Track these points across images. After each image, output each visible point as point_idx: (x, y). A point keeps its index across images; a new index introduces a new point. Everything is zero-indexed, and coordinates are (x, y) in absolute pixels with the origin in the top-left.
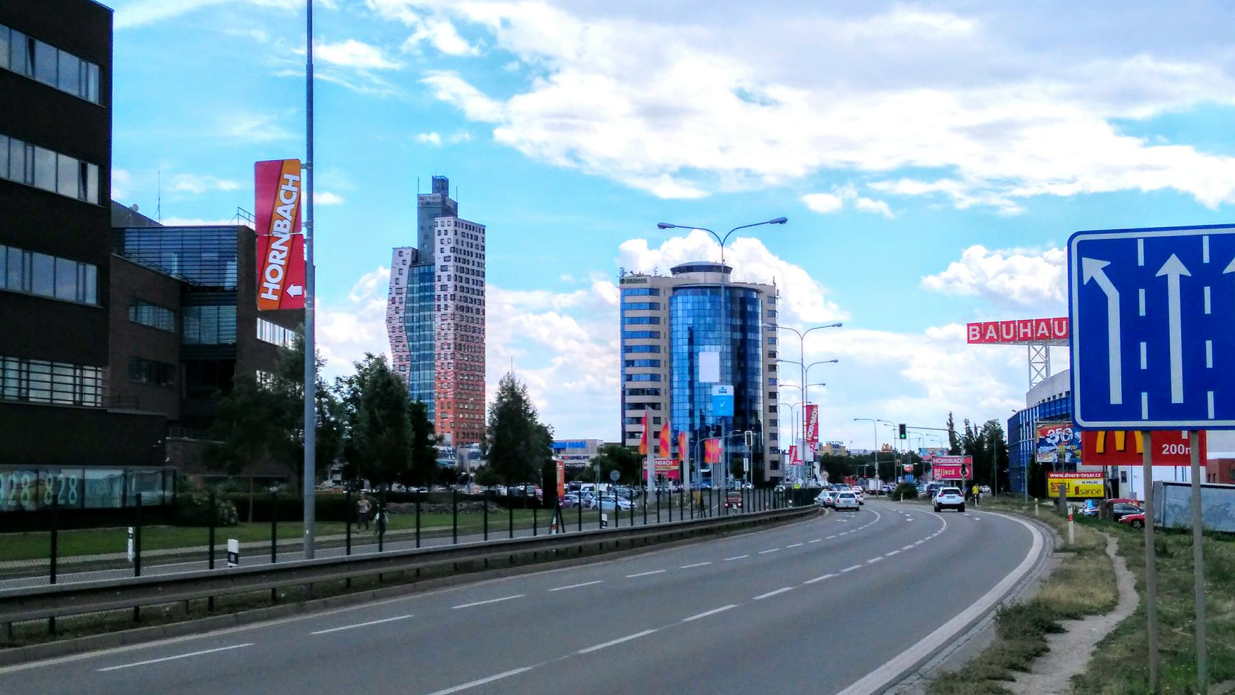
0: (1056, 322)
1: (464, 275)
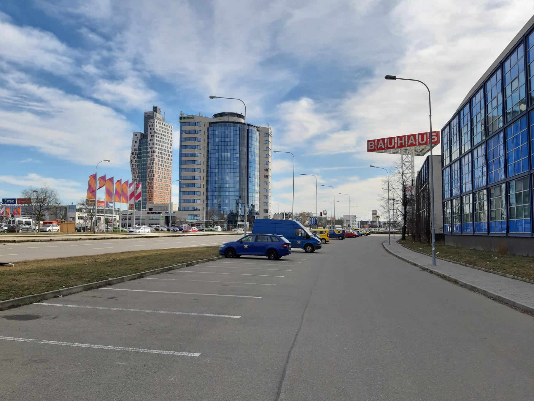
0: (388, 140)
1: (169, 146)
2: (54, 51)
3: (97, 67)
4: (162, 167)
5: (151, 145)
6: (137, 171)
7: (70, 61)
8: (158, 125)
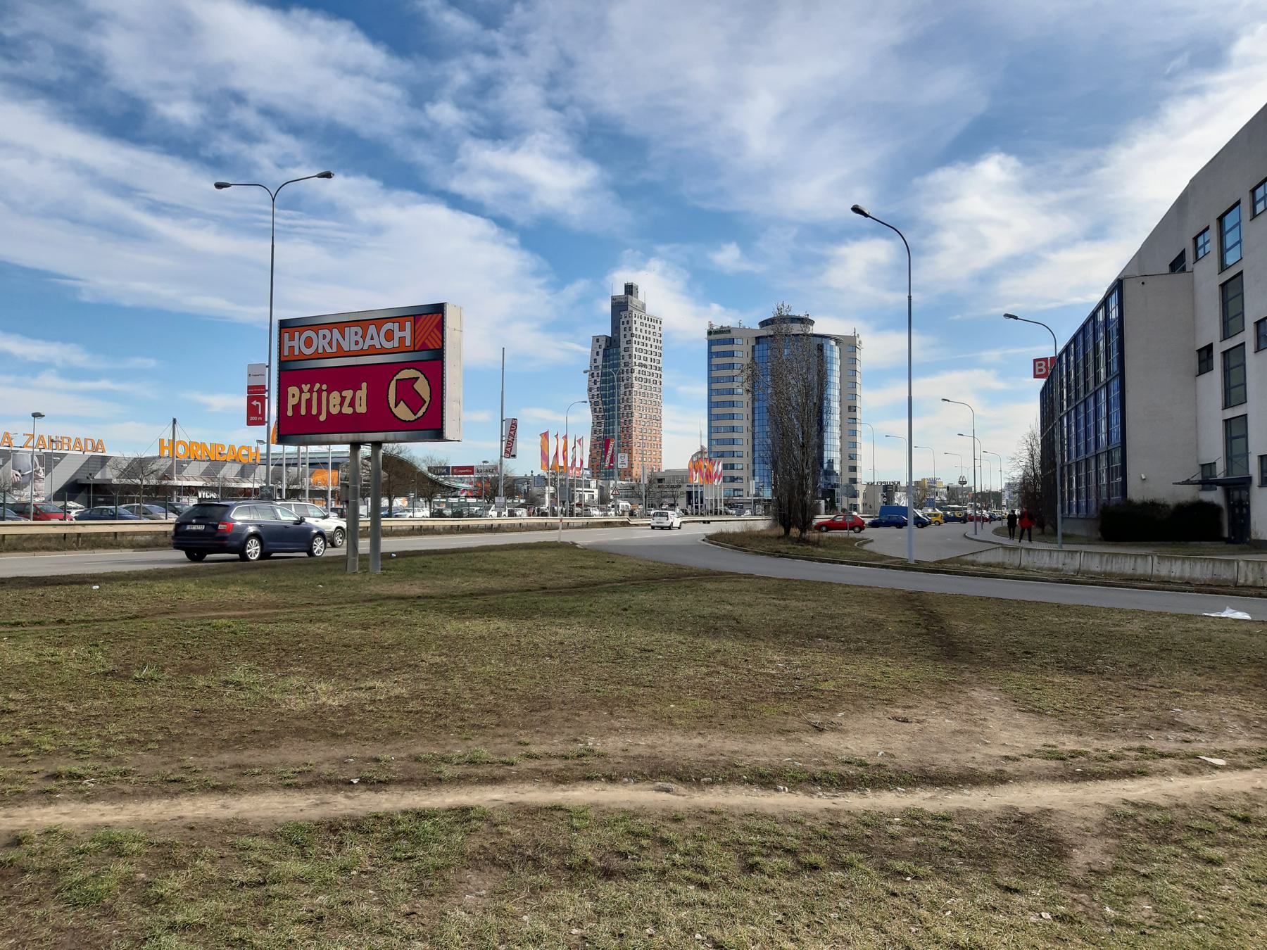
1: (657, 358)
2: (357, 71)
3: (460, 106)
4: (646, 398)
5: (627, 358)
6: (601, 406)
7: (396, 92)
8: (639, 321)
